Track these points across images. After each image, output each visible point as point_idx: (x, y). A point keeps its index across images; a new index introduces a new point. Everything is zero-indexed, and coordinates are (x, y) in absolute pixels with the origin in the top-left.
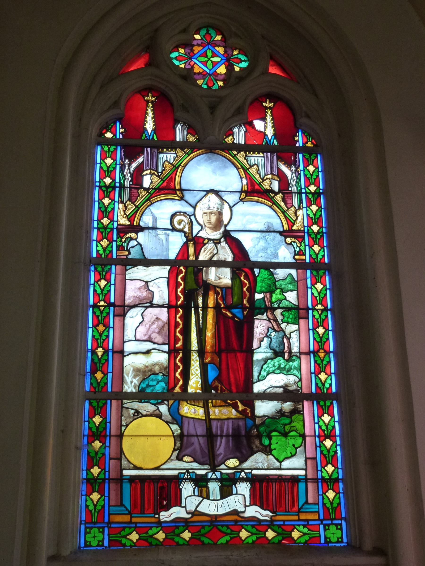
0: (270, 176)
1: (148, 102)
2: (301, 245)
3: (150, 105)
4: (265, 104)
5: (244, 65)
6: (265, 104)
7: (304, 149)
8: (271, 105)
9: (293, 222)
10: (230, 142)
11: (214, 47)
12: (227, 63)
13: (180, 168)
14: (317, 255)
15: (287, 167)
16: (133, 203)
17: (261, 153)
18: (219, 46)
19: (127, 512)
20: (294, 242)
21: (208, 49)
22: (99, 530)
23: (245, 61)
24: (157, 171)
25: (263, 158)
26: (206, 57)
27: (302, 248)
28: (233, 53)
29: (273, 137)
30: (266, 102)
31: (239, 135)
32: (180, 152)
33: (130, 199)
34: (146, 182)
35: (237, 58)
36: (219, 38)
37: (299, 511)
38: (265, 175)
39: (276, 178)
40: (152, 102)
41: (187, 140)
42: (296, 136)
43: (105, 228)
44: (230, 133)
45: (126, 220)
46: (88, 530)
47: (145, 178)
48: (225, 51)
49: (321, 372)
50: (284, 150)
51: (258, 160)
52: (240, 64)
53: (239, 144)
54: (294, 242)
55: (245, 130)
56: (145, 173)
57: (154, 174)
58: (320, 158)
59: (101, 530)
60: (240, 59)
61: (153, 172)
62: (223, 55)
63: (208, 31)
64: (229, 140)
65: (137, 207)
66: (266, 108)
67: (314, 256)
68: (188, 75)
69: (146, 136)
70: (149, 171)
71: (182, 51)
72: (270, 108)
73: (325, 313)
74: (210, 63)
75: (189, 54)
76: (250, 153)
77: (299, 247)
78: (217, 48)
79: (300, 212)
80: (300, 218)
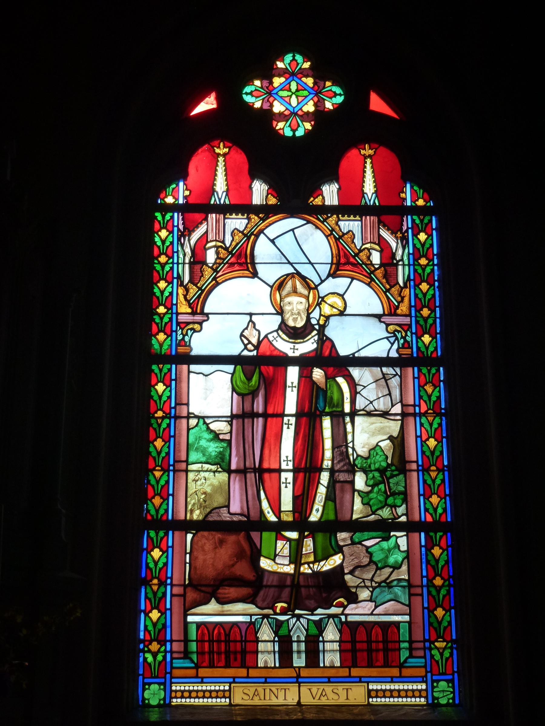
0: (368, 246)
1: (365, 157)
2: (406, 335)
3: (369, 161)
4: (217, 151)
5: (339, 100)
6: (363, 152)
7: (414, 210)
8: (371, 152)
9: (397, 304)
10: (320, 203)
11: (300, 79)
12: (316, 99)
13: (253, 237)
14: (427, 348)
15: (392, 234)
16: (196, 285)
17: (358, 216)
18: (307, 76)
19: (193, 665)
20: (399, 332)
21: (292, 81)
22: (160, 687)
23: (340, 95)
24: (223, 242)
25: (360, 223)
26: (290, 90)
27: (408, 339)
28: (325, 84)
29: (374, 195)
30: (219, 147)
31: (330, 194)
32: (255, 218)
33: (191, 281)
34: (211, 257)
35: (331, 90)
36: (307, 65)
37: (401, 666)
38: (363, 244)
39: (377, 247)
40: (224, 155)
41: (267, 203)
42: (403, 192)
43: (426, 319)
44: (317, 191)
45: (186, 306)
46: (435, 684)
47: (209, 252)
48: (315, 83)
49: (432, 494)
50: (388, 213)
51: (351, 225)
52: (333, 99)
53: (225, 205)
54: (399, 332)
55: (338, 187)
56: (209, 245)
57: (221, 247)
58: (436, 221)
59: (147, 687)
60: (335, 92)
61: (220, 244)
62: (312, 88)
63: (294, 56)
64: (318, 201)
65: (200, 289)
66: (219, 155)
67: (423, 349)
68: (266, 116)
69: (215, 200)
70: (214, 243)
71: (257, 83)
72: (370, 156)
73: (167, 421)
74: (291, 97)
75: (267, 88)
76: (343, 216)
77: (184, 336)
78: (304, 79)
79: (406, 292)
80: (406, 300)
